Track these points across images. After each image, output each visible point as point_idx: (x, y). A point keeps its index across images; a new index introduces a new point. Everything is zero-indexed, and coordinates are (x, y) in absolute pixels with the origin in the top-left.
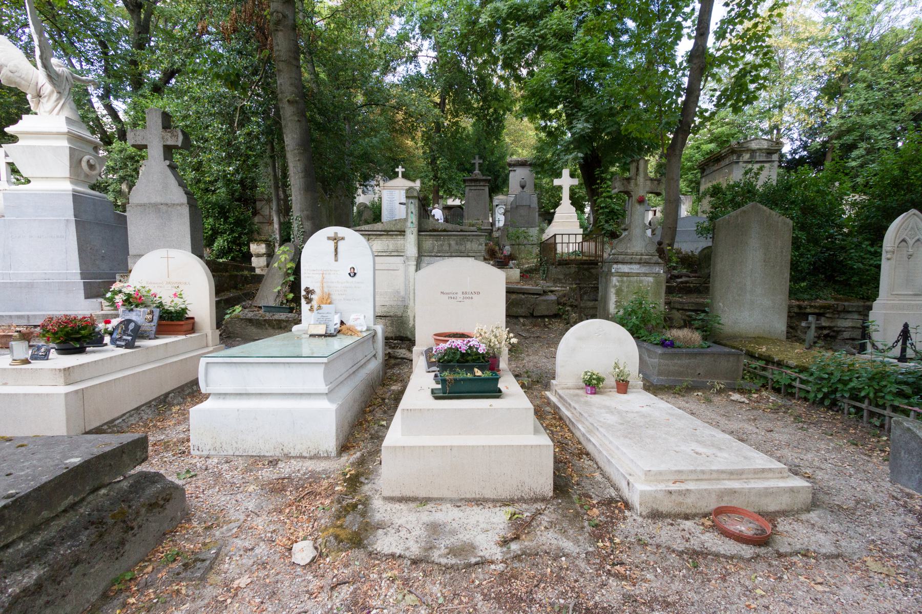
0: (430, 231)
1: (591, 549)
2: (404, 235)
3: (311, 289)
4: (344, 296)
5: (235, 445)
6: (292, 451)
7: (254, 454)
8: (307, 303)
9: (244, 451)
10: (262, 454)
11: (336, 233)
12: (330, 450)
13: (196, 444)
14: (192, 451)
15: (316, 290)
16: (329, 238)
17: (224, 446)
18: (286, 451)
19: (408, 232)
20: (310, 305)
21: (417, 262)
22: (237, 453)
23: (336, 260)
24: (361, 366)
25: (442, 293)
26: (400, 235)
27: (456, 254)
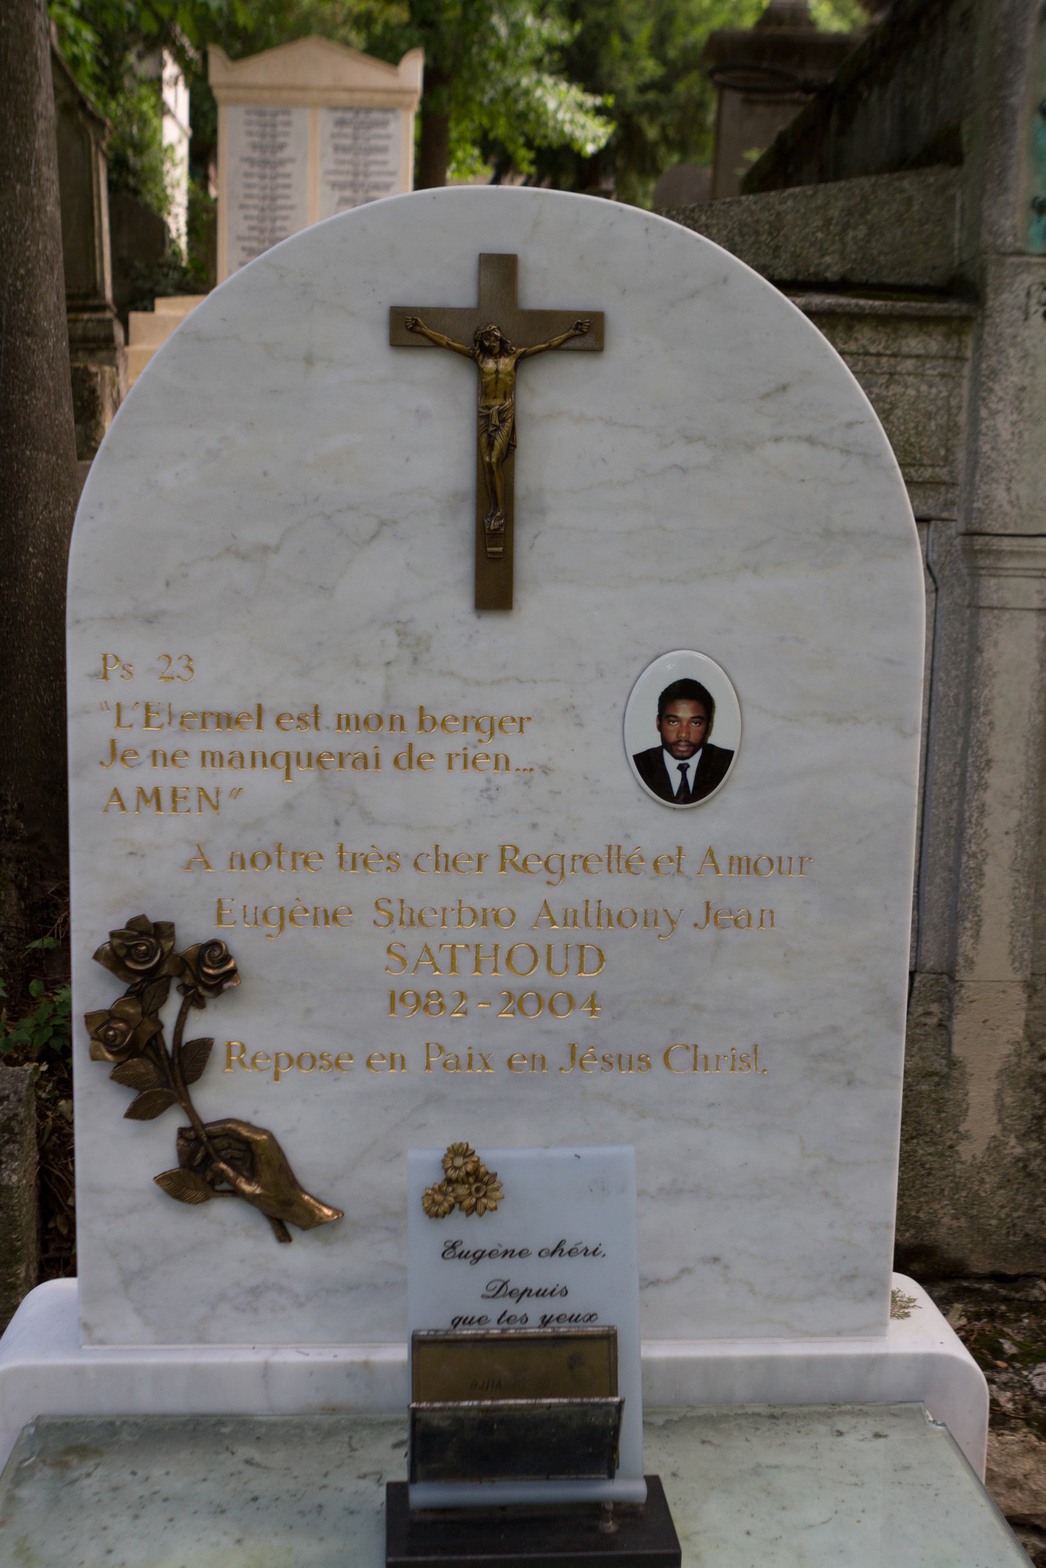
20: (174, 1121)
26: (923, 322)
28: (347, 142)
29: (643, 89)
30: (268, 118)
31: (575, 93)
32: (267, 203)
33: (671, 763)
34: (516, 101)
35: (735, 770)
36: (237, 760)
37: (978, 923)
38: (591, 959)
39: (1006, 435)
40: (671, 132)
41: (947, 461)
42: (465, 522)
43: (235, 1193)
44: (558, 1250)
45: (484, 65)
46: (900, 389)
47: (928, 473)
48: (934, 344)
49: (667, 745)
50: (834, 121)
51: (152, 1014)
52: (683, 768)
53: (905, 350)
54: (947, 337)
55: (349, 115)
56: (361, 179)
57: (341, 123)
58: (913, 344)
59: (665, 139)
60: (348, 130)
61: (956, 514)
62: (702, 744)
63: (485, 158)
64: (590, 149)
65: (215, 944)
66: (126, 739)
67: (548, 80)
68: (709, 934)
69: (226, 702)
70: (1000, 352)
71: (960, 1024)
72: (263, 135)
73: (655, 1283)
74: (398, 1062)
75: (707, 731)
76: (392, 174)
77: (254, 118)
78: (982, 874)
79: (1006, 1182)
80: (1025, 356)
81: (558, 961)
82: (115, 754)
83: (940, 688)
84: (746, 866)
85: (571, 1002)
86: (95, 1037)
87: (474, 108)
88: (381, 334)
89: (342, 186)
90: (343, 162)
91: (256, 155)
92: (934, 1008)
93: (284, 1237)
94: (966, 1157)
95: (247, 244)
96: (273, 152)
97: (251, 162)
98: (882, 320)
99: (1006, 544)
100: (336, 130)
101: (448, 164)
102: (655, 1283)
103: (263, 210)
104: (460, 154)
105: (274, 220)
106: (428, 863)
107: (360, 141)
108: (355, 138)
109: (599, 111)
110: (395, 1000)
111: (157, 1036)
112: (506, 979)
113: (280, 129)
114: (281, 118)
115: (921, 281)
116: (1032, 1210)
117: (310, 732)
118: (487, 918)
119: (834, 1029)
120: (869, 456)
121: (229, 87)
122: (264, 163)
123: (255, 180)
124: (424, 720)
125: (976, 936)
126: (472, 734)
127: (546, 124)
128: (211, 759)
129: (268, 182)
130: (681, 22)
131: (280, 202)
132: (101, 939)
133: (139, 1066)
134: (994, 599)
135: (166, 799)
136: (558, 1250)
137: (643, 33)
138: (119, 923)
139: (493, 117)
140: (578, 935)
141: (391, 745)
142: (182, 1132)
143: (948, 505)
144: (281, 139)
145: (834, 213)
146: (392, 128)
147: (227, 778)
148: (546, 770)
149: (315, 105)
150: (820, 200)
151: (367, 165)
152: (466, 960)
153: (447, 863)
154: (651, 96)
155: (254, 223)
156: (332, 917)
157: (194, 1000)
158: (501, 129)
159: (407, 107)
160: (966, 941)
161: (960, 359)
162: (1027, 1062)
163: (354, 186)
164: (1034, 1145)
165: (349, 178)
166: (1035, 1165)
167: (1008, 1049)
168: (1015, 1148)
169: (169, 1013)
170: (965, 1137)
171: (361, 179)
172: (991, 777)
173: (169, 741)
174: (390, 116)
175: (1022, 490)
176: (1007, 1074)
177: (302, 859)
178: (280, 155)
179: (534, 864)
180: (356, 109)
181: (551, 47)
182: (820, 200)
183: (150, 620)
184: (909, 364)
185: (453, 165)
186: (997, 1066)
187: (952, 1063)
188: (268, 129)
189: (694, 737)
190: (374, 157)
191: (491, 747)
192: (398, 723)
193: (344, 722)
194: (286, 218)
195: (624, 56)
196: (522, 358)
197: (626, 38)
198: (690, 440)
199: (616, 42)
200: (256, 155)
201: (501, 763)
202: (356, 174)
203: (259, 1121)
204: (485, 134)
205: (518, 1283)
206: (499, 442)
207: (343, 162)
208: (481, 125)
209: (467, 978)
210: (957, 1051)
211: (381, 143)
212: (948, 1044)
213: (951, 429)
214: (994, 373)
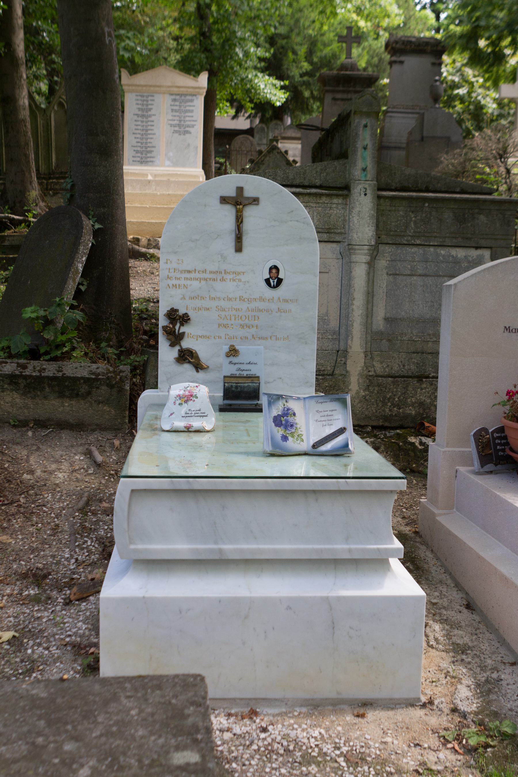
2: (346, 197)
3: (182, 311)
4: (253, 330)
8: (172, 345)
11: (240, 190)
16: (224, 200)
19: (357, 190)
20: (177, 348)
21: (371, 255)
23: (239, 249)
24: (314, 492)
25: (507, 329)
26: (337, 196)
28: (177, 108)
29: (301, 76)
30: (145, 98)
31: (273, 80)
32: (144, 132)
33: (271, 281)
34: (246, 85)
35: (283, 282)
36: (191, 279)
37: (352, 337)
38: (256, 318)
39: (356, 222)
40: (315, 93)
41: (344, 228)
42: (233, 236)
43: (190, 362)
44: (249, 363)
45: (232, 68)
47: (339, 231)
48: (340, 201)
49: (271, 277)
50: (330, 139)
51: (174, 327)
54: (343, 199)
55: (178, 97)
56: (182, 123)
57: (174, 100)
58: (335, 201)
59: (312, 96)
60: (177, 103)
61: (346, 240)
62: (277, 277)
63: (232, 105)
64: (278, 104)
65: (186, 314)
66: (170, 275)
67: (260, 75)
68: (279, 314)
69: (189, 268)
70: (354, 203)
71: (349, 362)
72: (143, 105)
73: (269, 383)
74: (220, 337)
76: (195, 121)
77: (139, 98)
78: (353, 326)
79: (360, 401)
80: (360, 204)
81: (250, 319)
82: (169, 278)
83: (343, 282)
84: (286, 301)
85: (253, 327)
86: (164, 330)
87: (227, 85)
88: (218, 201)
89: (175, 126)
90: (175, 116)
91: (140, 113)
92: (343, 359)
93: (198, 371)
95: (136, 149)
96: (147, 112)
97: (138, 115)
98: (327, 195)
99: (357, 247)
100: (173, 103)
101: (216, 109)
102: (269, 383)
103: (142, 135)
104: (221, 105)
105: (147, 139)
106: (226, 299)
107: (182, 108)
108: (180, 106)
109: (282, 88)
110: (219, 325)
111: (175, 331)
112: (240, 322)
113: (150, 102)
114: (150, 98)
115: (339, 186)
116: (367, 409)
117: (204, 274)
118: (237, 310)
119: (303, 333)
120: (308, 224)
121: (129, 85)
122: (143, 116)
123: (139, 123)
124: (226, 272)
125: (352, 340)
126: (234, 275)
127: (259, 94)
128: (186, 279)
129: (144, 124)
130: (319, 46)
131: (149, 132)
132: (165, 312)
133: (171, 337)
134: (354, 260)
136: (249, 363)
137: (302, 51)
138: (169, 309)
139: (235, 90)
140: (254, 313)
141: (219, 277)
143: (344, 238)
144: (150, 107)
145: (318, 170)
146: (195, 102)
147: (189, 282)
148: (248, 282)
149: (164, 93)
150: (315, 167)
151: (184, 117)
152: (233, 318)
153: (230, 299)
154: (305, 78)
155: (139, 140)
156: (208, 309)
157: (182, 325)
158: (239, 95)
159: (202, 95)
160: (349, 342)
161: (346, 204)
162: (365, 372)
163: (179, 126)
165: (177, 122)
166: (367, 397)
167: (360, 368)
168: (362, 393)
169: (177, 327)
171: (182, 123)
172: (355, 302)
173: (178, 275)
174: (194, 98)
175: (360, 234)
176: (360, 375)
177: (203, 298)
178: (149, 113)
179: (246, 300)
180: (181, 95)
181: (260, 59)
182: (315, 167)
183: (175, 253)
184: (335, 206)
185: (218, 110)
186: (357, 373)
187: (347, 372)
188: (145, 103)
190: (187, 114)
191: (238, 277)
192: (221, 273)
193: (211, 272)
194: (152, 138)
195: (294, 61)
196: (244, 206)
197: (295, 53)
198: (275, 221)
199: (290, 54)
200: (140, 113)
201: (240, 280)
202: (180, 121)
203: (193, 348)
204: (232, 96)
205: (242, 368)
206: (240, 221)
207: (175, 116)
208: (230, 92)
209: (233, 322)
210: (348, 369)
211: (191, 108)
212: (346, 368)
213: (344, 220)
214: (353, 208)
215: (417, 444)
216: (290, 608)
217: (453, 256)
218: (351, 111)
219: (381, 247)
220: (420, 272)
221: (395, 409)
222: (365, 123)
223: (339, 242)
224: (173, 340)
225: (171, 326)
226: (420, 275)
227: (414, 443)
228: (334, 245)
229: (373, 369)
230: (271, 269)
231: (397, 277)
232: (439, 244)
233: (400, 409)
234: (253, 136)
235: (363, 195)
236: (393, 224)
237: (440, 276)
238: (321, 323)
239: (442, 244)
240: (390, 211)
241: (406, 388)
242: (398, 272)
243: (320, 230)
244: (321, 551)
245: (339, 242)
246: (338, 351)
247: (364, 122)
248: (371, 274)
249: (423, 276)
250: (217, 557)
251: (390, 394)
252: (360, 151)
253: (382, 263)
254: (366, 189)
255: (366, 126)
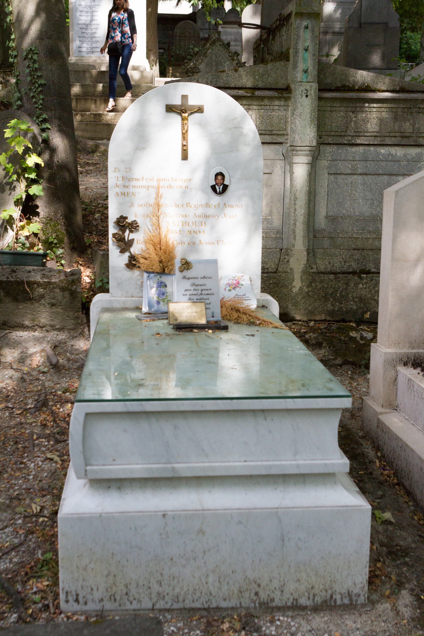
0: (337, 90)
1: (46, 578)
5: (156, 588)
6: (277, 596)
7: (197, 605)
8: (122, 251)
9: (176, 599)
10: (214, 605)
12: (356, 591)
13: (73, 588)
14: (63, 606)
15: (140, 222)
17: (133, 591)
18: (263, 596)
20: (127, 254)
22: (161, 605)
24: (263, 411)
26: (279, 98)
27: (394, 141)
33: (217, 187)
38: (203, 224)
39: (298, 124)
41: (286, 130)
46: (275, 113)
47: (282, 132)
48: (282, 103)
49: (216, 184)
50: (271, 37)
52: (219, 188)
53: (275, 104)
58: (277, 103)
62: (223, 184)
75: (224, 181)
81: (197, 224)
86: (114, 237)
92: (286, 257)
94: (294, 291)
111: (124, 238)
132: (115, 220)
135: (126, 194)
142: (129, 257)
157: (131, 231)
164: (310, 289)
166: (310, 294)
167: (303, 266)
170: (294, 287)
176: (304, 272)
179: (193, 206)
186: (300, 270)
189: (221, 182)
215: (358, 339)
216: (241, 523)
217: (392, 155)
218: (292, 12)
219: (322, 148)
220: (360, 171)
221: (337, 304)
222: (306, 24)
223: (281, 143)
224: (123, 246)
225: (121, 233)
226: (360, 174)
227: (355, 338)
228: (277, 147)
229: (315, 267)
230: (217, 175)
231: (338, 176)
232: (379, 143)
233: (341, 304)
234: (195, 22)
235: (304, 97)
236: (334, 124)
237: (380, 174)
238: (265, 223)
239: (382, 143)
240: (331, 111)
241: (347, 284)
242: (339, 172)
243: (263, 132)
244: (271, 467)
245: (281, 143)
246: (281, 250)
247: (305, 23)
248: (313, 175)
249: (363, 174)
250: (170, 475)
251: (332, 290)
252: (301, 52)
253: (323, 163)
254: (307, 90)
255: (307, 27)
